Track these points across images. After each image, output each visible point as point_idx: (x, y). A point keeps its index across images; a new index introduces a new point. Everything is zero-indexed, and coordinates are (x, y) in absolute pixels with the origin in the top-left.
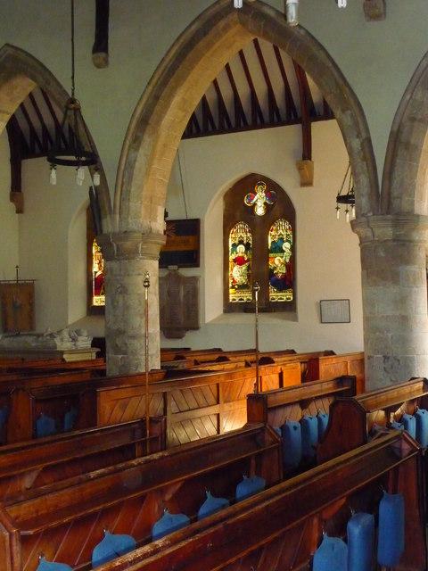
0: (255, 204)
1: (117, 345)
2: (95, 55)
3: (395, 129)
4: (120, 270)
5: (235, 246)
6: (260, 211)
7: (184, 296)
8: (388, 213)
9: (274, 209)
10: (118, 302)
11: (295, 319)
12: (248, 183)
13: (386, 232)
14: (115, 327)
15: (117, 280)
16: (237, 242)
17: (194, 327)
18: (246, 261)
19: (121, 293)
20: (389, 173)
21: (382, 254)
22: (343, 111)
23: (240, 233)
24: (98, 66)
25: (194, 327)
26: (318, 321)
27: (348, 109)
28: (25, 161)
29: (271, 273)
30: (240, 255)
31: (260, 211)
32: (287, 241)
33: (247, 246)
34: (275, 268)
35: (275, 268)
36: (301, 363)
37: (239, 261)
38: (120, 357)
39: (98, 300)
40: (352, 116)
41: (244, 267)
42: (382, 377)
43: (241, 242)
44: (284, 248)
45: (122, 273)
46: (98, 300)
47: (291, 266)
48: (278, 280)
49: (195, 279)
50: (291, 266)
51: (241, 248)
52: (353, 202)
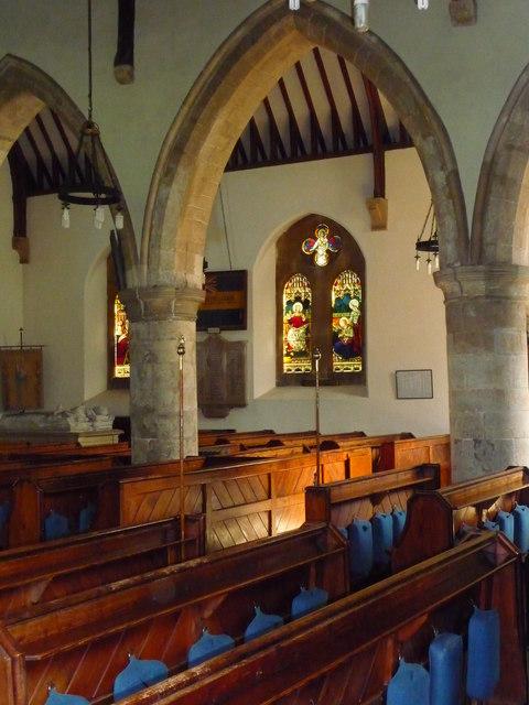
0: (315, 252)
1: (144, 426)
2: (118, 68)
3: (489, 159)
4: (149, 333)
5: (290, 303)
6: (321, 260)
7: (228, 366)
8: (479, 263)
9: (339, 258)
10: (145, 373)
11: (365, 394)
12: (306, 227)
13: (477, 286)
14: (142, 404)
15: (145, 346)
16: (293, 299)
17: (240, 403)
18: (304, 323)
19: (149, 361)
20: (481, 213)
21: (472, 314)
22: (424, 137)
23: (297, 288)
24: (122, 82)
25: (240, 403)
26: (394, 396)
27: (430, 134)
28: (31, 198)
29: (335, 337)
30: (297, 314)
31: (321, 260)
32: (355, 297)
33: (305, 304)
34: (340, 331)
35: (340, 331)
36: (372, 448)
37: (296, 322)
38: (149, 440)
39: (121, 371)
40: (435, 143)
41: (302, 330)
42: (472, 465)
43: (298, 299)
44: (351, 307)
45: (151, 337)
46: (121, 371)
47: (360, 329)
48: (343, 346)
49: (241, 345)
50: (360, 329)
51: (298, 307)
52: (436, 250)
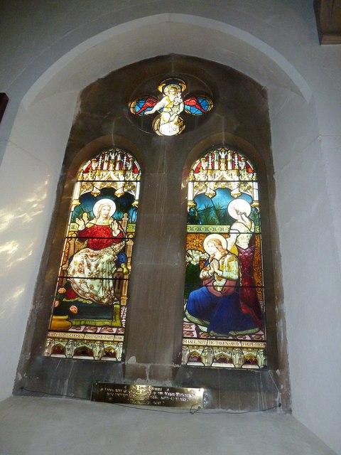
0: (157, 114)
5: (88, 199)
6: (168, 127)
9: (212, 119)
11: (286, 404)
12: (141, 79)
16: (96, 191)
18: (120, 239)
23: (111, 173)
28: (175, 133)
29: (192, 276)
30: (101, 222)
31: (168, 127)
32: (241, 195)
33: (124, 203)
34: (205, 263)
35: (205, 263)
36: (321, 44)
37: (95, 239)
41: (107, 255)
43: (107, 192)
44: (232, 213)
47: (260, 263)
48: (210, 296)
50: (260, 263)
51: (104, 210)
52: (188, 215)
